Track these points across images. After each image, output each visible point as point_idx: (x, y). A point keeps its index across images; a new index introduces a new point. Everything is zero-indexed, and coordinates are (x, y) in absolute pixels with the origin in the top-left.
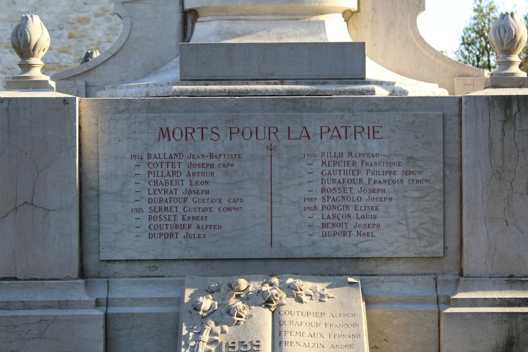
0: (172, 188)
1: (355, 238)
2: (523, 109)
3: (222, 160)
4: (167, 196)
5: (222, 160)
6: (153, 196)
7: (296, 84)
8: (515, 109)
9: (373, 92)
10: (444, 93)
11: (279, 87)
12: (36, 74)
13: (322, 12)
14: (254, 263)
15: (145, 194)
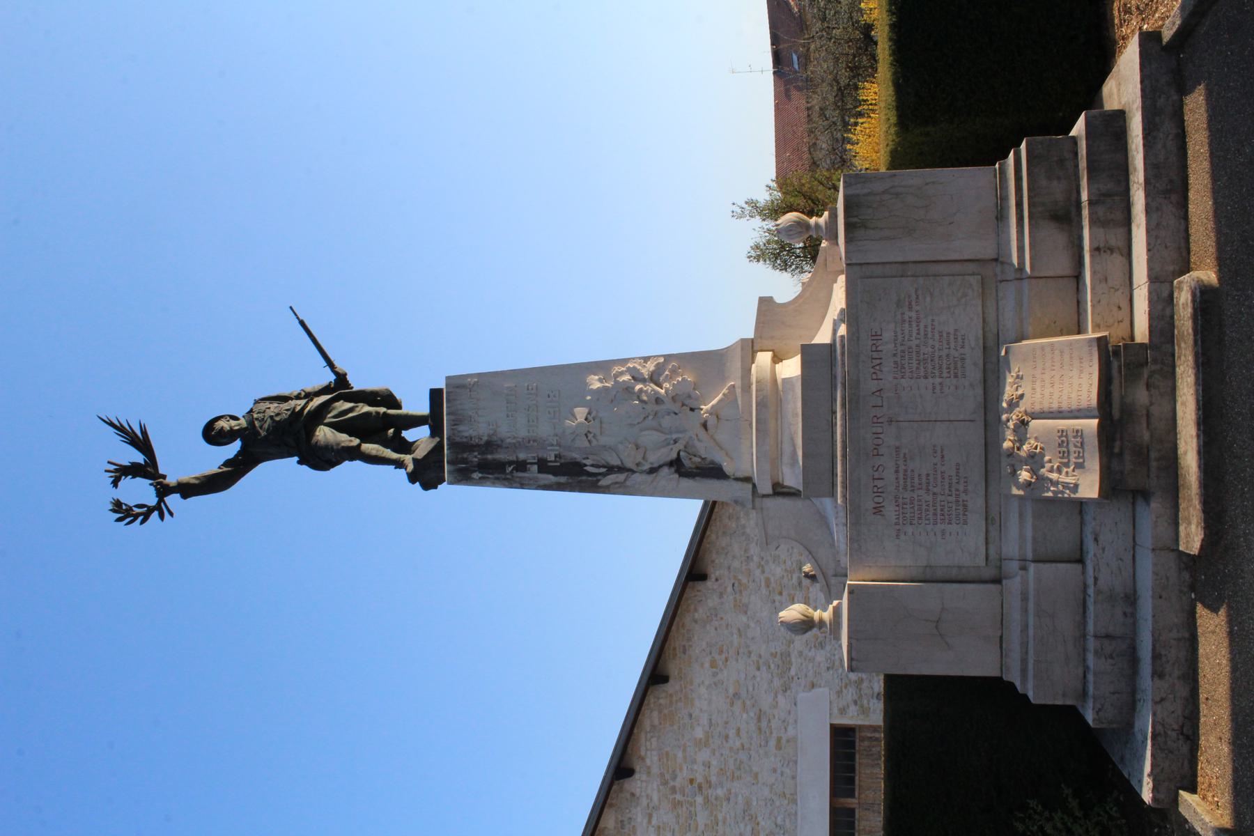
4: (931, 509)
5: (901, 462)
8: (855, 220)
9: (842, 337)
10: (842, 279)
11: (839, 415)
12: (827, 615)
13: (774, 380)
15: (929, 528)
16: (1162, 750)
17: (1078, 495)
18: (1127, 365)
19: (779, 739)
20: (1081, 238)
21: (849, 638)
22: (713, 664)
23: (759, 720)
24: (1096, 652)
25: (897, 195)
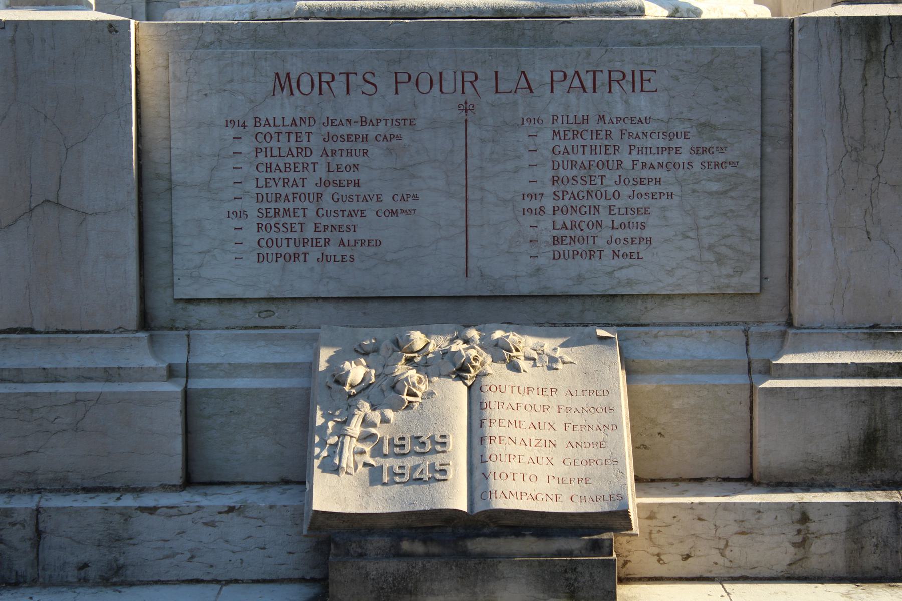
0: (297, 176)
3: (382, 128)
4: (288, 191)
5: (382, 128)
6: (264, 191)
8: (885, 39)
14: (437, 304)
15: (250, 186)
17: (317, 473)
18: (573, 568)
20: (828, 487)
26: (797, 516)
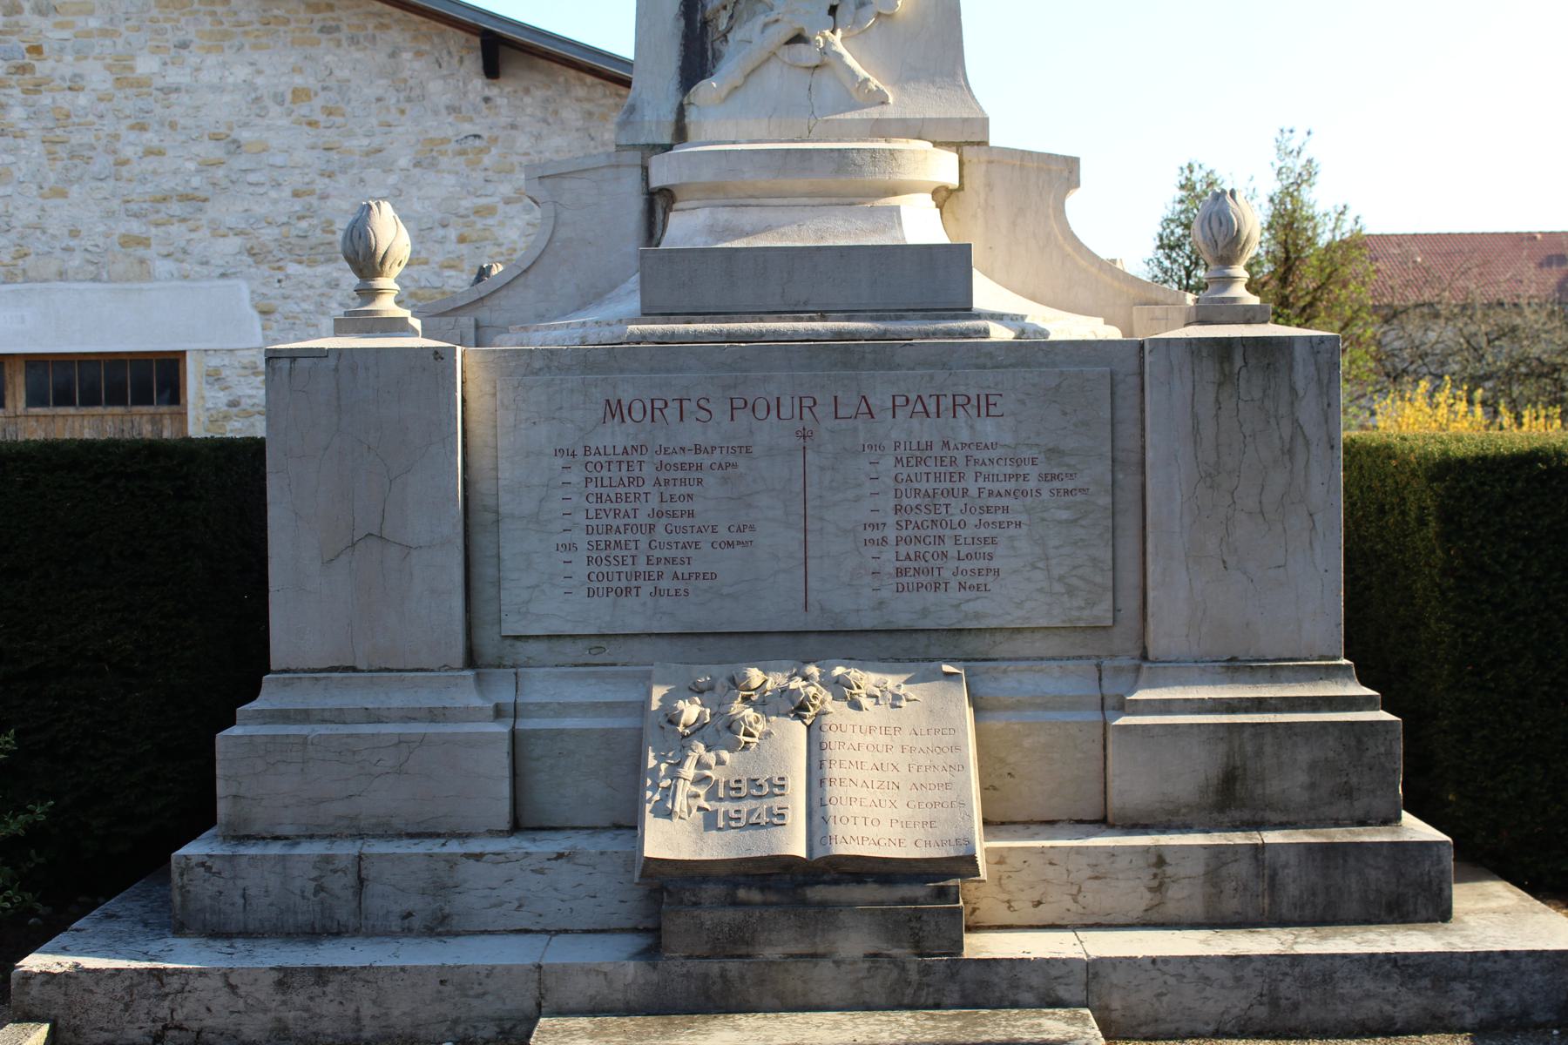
0: (629, 507)
1: (956, 595)
2: (1252, 362)
3: (717, 457)
4: (620, 522)
5: (717, 457)
6: (594, 522)
7: (849, 319)
9: (986, 333)
10: (1114, 334)
11: (818, 325)
12: (387, 306)
14: (776, 640)
15: (580, 517)
16: (130, 990)
17: (649, 817)
18: (918, 916)
19: (144, 242)
20: (1186, 828)
21: (340, 352)
22: (300, 95)
23: (185, 198)
24: (327, 859)
25: (1290, 453)
26: (1153, 860)
